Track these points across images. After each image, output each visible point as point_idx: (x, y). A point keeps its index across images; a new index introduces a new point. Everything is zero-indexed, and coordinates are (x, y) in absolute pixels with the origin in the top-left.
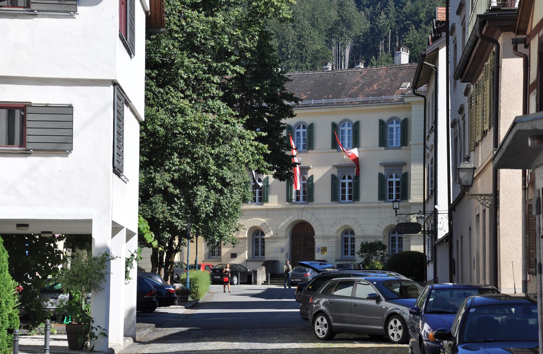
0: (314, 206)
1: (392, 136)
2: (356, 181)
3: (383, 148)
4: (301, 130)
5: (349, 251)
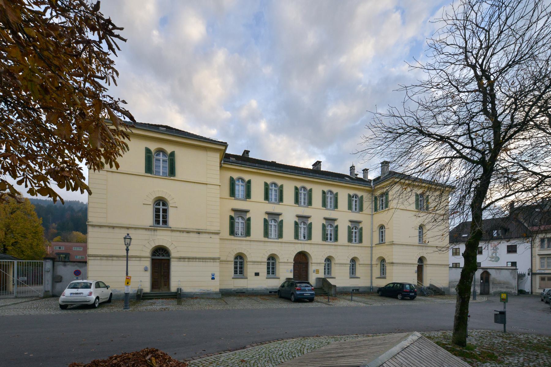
5: (271, 272)
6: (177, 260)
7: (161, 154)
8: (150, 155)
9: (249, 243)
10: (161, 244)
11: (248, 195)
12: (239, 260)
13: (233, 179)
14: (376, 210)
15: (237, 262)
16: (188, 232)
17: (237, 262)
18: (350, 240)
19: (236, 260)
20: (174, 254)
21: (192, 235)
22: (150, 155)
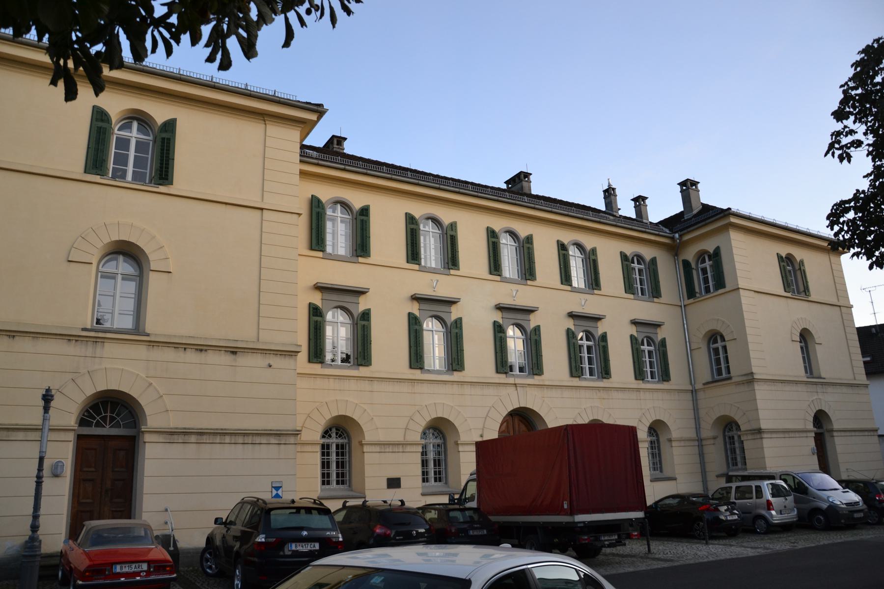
5: (432, 475)
6: (160, 438)
7: (135, 125)
8: (103, 125)
9: (366, 385)
10: (113, 385)
11: (361, 246)
12: (334, 441)
13: (319, 201)
14: (691, 293)
15: (328, 446)
16: (201, 349)
17: (328, 446)
18: (639, 374)
19: (326, 441)
20: (153, 419)
21: (212, 358)
22: (103, 125)
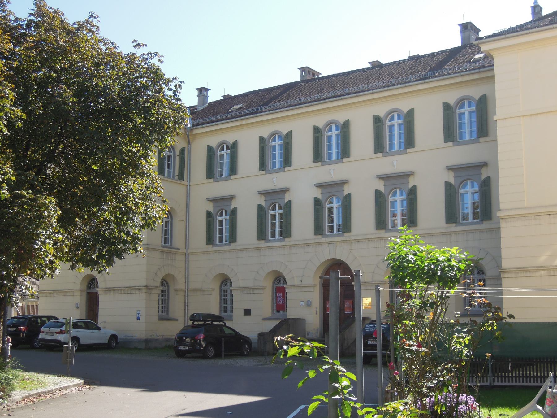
0: (352, 238)
1: (391, 137)
2: (411, 196)
3: (451, 144)
4: (225, 152)
